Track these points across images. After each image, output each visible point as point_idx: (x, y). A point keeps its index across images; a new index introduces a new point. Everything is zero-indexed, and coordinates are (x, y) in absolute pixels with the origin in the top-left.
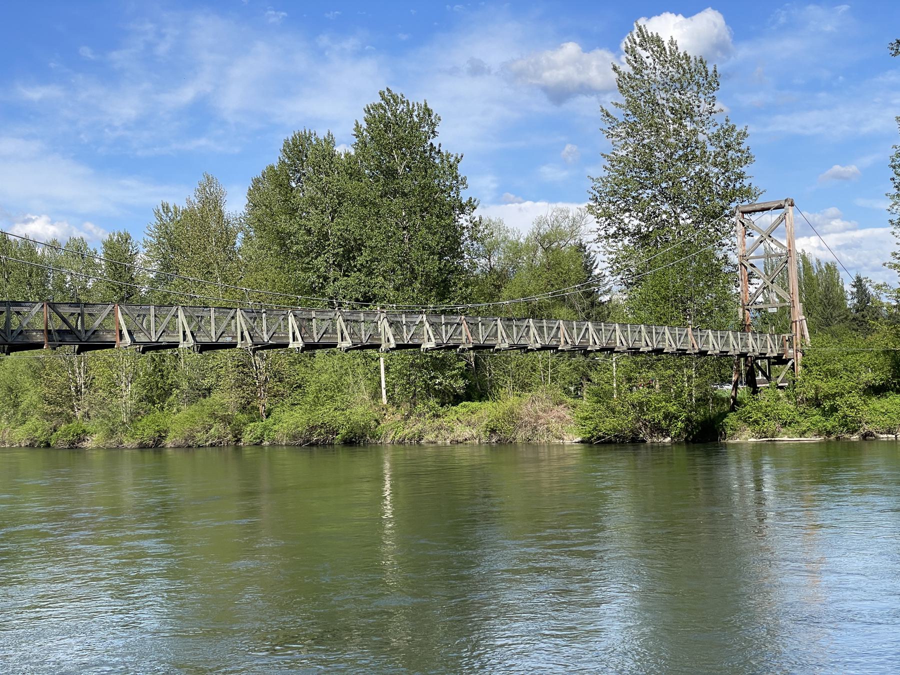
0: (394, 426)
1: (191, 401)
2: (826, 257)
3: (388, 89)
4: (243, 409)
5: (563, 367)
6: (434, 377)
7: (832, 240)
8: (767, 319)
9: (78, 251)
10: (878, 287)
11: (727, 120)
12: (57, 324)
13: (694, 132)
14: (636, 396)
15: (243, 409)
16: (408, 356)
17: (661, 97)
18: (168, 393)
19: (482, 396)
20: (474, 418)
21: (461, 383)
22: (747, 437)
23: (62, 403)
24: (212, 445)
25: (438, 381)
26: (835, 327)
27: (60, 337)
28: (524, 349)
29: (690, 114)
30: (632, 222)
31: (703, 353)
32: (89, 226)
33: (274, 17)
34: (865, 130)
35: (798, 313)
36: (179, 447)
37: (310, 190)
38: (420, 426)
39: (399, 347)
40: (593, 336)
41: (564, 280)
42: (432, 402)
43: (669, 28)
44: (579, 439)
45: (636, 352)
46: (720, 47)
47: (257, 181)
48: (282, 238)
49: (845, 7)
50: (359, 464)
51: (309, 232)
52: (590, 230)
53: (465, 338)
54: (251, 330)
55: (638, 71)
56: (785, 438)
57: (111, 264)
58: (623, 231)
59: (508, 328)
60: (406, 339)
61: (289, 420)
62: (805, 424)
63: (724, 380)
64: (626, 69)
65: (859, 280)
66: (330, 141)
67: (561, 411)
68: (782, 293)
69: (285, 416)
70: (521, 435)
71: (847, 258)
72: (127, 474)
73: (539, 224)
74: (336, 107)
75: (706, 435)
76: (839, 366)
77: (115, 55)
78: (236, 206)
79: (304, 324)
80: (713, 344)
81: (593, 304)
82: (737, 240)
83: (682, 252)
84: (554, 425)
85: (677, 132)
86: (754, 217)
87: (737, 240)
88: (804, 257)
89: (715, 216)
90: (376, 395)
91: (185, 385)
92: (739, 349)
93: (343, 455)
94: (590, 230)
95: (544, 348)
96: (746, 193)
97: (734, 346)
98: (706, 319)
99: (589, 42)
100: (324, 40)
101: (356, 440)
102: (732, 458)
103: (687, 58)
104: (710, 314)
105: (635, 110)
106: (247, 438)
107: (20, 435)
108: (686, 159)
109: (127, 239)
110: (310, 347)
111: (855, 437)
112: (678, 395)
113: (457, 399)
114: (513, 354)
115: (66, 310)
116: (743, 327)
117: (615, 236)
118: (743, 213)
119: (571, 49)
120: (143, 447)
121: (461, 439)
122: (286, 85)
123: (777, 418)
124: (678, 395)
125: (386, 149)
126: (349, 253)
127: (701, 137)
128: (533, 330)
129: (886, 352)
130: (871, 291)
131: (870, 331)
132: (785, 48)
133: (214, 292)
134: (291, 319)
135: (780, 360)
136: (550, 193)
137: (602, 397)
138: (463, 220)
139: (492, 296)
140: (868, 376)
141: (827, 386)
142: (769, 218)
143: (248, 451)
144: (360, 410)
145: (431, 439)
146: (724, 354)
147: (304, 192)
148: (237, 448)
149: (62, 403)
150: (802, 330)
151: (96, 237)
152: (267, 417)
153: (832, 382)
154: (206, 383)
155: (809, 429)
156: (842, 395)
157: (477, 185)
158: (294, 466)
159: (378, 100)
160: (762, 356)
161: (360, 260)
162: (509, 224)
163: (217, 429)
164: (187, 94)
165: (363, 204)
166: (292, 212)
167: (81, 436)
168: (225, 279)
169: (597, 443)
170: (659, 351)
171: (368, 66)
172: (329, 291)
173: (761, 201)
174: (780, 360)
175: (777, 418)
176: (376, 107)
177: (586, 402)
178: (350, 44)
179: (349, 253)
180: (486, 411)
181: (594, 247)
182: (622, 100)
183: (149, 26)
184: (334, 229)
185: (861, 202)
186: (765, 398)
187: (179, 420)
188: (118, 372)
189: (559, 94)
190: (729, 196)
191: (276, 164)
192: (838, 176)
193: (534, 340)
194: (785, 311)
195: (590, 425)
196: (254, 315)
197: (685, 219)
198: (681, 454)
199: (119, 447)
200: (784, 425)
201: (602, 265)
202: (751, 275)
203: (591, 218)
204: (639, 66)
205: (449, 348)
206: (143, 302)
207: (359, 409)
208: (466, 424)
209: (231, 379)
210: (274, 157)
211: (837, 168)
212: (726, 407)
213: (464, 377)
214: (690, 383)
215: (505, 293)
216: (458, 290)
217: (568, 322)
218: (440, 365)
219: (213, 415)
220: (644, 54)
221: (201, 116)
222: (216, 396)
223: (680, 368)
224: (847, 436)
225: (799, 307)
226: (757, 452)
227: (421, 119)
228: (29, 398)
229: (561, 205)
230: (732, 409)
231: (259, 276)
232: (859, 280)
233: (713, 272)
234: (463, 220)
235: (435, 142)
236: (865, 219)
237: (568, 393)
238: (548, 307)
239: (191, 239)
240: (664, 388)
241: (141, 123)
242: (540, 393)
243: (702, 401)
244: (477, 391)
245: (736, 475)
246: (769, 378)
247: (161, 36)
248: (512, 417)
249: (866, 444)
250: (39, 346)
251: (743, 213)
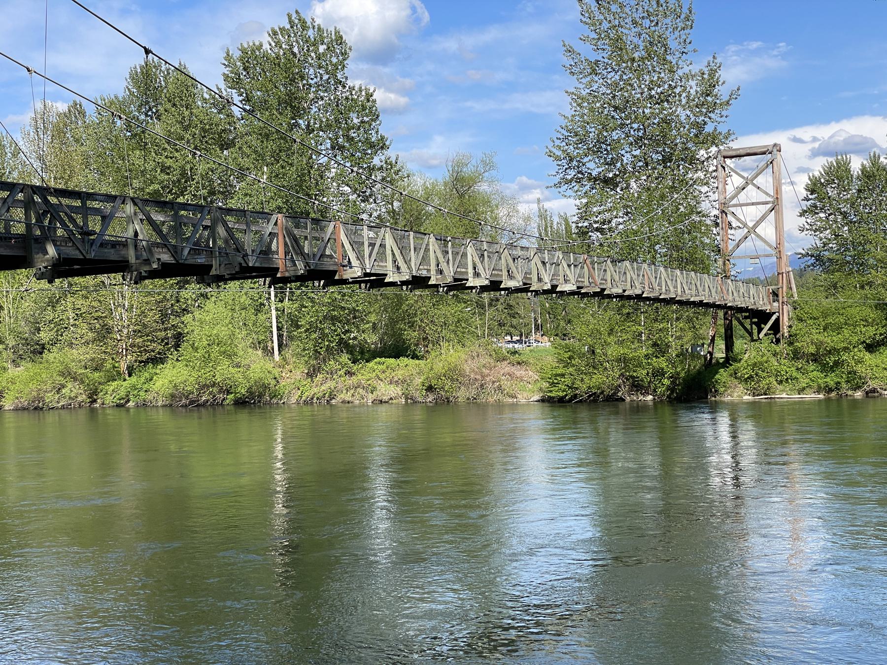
3: (297, 12)
6: (347, 331)
11: (714, 57)
24: (63, 407)
25: (352, 335)
36: (24, 409)
38: (331, 384)
42: (345, 358)
44: (537, 397)
56: (783, 394)
62: (804, 381)
70: (462, 394)
84: (506, 384)
93: (243, 416)
101: (254, 401)
111: (859, 394)
118: (725, 157)
121: (385, 398)
141: (830, 340)
145: (347, 399)
150: (789, 282)
152: (130, 375)
155: (809, 386)
163: (72, 389)
207: (256, 367)
224: (850, 393)
249: (871, 401)
251: (725, 157)
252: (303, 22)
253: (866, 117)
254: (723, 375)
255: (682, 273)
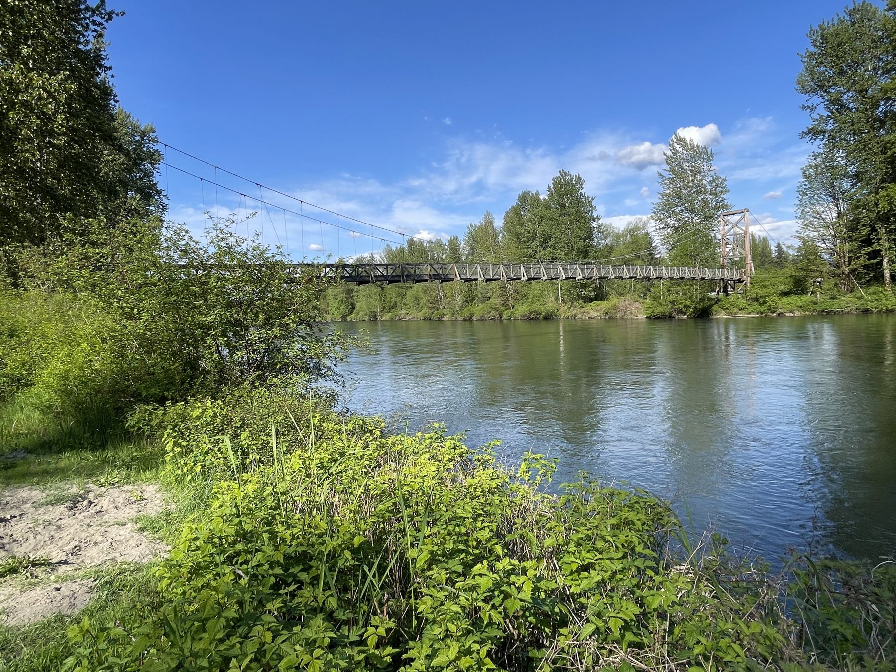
0: (564, 311)
1: (483, 302)
2: (763, 235)
4: (503, 305)
5: (638, 286)
7: (767, 227)
8: (733, 264)
9: (439, 244)
10: (788, 247)
12: (433, 272)
13: (701, 180)
14: (671, 298)
15: (503, 305)
16: (571, 282)
17: (686, 165)
18: (474, 299)
19: (602, 299)
20: (599, 308)
21: (593, 293)
22: (723, 315)
23: (435, 303)
26: (766, 266)
27: (435, 277)
28: (621, 278)
29: (700, 172)
30: (671, 222)
31: (703, 279)
32: (443, 234)
33: (508, 143)
34: (780, 175)
35: (749, 260)
37: (529, 215)
39: (567, 279)
40: (653, 272)
41: (638, 247)
42: (581, 301)
43: (694, 135)
45: (672, 279)
46: (716, 141)
47: (507, 212)
48: (518, 236)
49: (770, 118)
50: (550, 327)
51: (529, 233)
52: (652, 227)
53: (595, 274)
54: (506, 273)
55: (675, 154)
56: (740, 315)
57: (452, 249)
58: (667, 226)
59: (614, 270)
60: (570, 275)
61: (522, 309)
62: (751, 309)
63: (713, 290)
64: (669, 153)
65: (779, 244)
66: (537, 194)
67: (637, 304)
68: (742, 251)
69: (519, 308)
70: (619, 315)
71: (772, 234)
72: (459, 331)
73: (629, 225)
74: (538, 178)
75: (703, 314)
76: (768, 283)
77: (445, 165)
78: (499, 223)
79: (527, 270)
80: (708, 274)
81: (652, 259)
82: (721, 228)
83: (694, 234)
84: (634, 310)
85: (693, 181)
86: (729, 217)
87: (721, 228)
88: (752, 236)
89: (711, 217)
90: (557, 299)
91: (480, 296)
92: (721, 276)
93: (544, 323)
94: (652, 227)
95: (630, 278)
96: (725, 206)
97: (718, 275)
98: (705, 264)
99: (654, 142)
100: (528, 151)
101: (548, 317)
102: (715, 324)
103: (698, 146)
104: (707, 261)
105: (673, 171)
106: (505, 316)
107: (420, 315)
108: (698, 192)
109: (457, 239)
110: (529, 279)
111: (774, 315)
112: (691, 297)
113: (591, 300)
114: (616, 281)
115: (435, 267)
116: (723, 267)
117: (663, 228)
119: (647, 145)
120: (465, 320)
122: (513, 172)
123: (737, 306)
124: (691, 297)
125: (561, 196)
126: (546, 239)
127: (704, 182)
128: (625, 270)
129: (791, 277)
130: (785, 249)
131: (783, 267)
132: (740, 140)
133: (491, 258)
134: (522, 268)
135: (740, 281)
136: (631, 212)
137: (655, 298)
138: (595, 225)
139: (607, 257)
140: (782, 288)
141: (761, 292)
142: (737, 217)
143: (505, 321)
144: (550, 305)
146: (713, 279)
147: (526, 215)
148: (501, 321)
149: (435, 303)
151: (445, 239)
153: (764, 290)
154: (489, 295)
156: (768, 296)
157: (600, 209)
158: (523, 327)
159: (558, 175)
160: (731, 280)
161: (550, 243)
162: (614, 225)
163: (493, 312)
164: (474, 178)
165: (551, 219)
166: (522, 225)
167: (442, 315)
168: (495, 253)
169: (654, 318)
170: (683, 278)
171: (548, 161)
172: (537, 256)
173: (733, 210)
174: (740, 281)
175: (737, 306)
176: (557, 178)
177: (648, 301)
178: (540, 151)
179: (546, 239)
180: (604, 305)
181: (653, 234)
182: (668, 168)
183: (457, 152)
184: (539, 230)
185: (781, 209)
186: (731, 298)
187: (478, 309)
188: (456, 290)
189: (641, 166)
190: (717, 208)
191: (515, 205)
192: (772, 197)
193: (626, 274)
194: (743, 259)
195: (650, 311)
196: (507, 267)
197: (696, 219)
198: (692, 321)
199: (456, 320)
200: (740, 310)
201: (657, 241)
202: (727, 243)
203: (652, 221)
204: (676, 152)
205: (588, 279)
206: (463, 263)
207: (550, 304)
208: (595, 311)
209: (498, 293)
210: (514, 202)
211: (771, 193)
212: (713, 302)
213: (594, 291)
214: (696, 291)
215: (613, 255)
216: (592, 254)
217: (641, 266)
218: (584, 286)
219: (491, 307)
220: (678, 146)
221: (480, 187)
222: (492, 300)
223: (692, 285)
225: (749, 257)
226: (727, 322)
227: (577, 182)
228: (423, 301)
229: (638, 216)
230: (716, 303)
231: (509, 251)
232: (779, 244)
233: (708, 243)
234: (595, 225)
235: (583, 191)
236: (781, 217)
237: (640, 297)
238: (632, 260)
239: (482, 237)
240: (685, 294)
241: (457, 192)
242: (628, 297)
243: (702, 300)
244: (600, 296)
245: (716, 331)
246: (734, 289)
247: (462, 155)
248: (615, 307)
250: (426, 280)
252: (565, 173)
253: (224, 208)
254: (716, 307)
255: (679, 270)
